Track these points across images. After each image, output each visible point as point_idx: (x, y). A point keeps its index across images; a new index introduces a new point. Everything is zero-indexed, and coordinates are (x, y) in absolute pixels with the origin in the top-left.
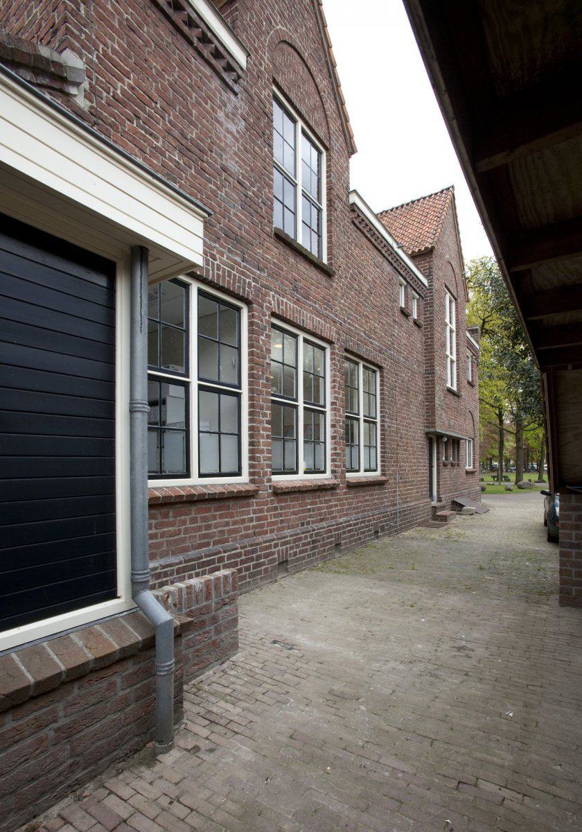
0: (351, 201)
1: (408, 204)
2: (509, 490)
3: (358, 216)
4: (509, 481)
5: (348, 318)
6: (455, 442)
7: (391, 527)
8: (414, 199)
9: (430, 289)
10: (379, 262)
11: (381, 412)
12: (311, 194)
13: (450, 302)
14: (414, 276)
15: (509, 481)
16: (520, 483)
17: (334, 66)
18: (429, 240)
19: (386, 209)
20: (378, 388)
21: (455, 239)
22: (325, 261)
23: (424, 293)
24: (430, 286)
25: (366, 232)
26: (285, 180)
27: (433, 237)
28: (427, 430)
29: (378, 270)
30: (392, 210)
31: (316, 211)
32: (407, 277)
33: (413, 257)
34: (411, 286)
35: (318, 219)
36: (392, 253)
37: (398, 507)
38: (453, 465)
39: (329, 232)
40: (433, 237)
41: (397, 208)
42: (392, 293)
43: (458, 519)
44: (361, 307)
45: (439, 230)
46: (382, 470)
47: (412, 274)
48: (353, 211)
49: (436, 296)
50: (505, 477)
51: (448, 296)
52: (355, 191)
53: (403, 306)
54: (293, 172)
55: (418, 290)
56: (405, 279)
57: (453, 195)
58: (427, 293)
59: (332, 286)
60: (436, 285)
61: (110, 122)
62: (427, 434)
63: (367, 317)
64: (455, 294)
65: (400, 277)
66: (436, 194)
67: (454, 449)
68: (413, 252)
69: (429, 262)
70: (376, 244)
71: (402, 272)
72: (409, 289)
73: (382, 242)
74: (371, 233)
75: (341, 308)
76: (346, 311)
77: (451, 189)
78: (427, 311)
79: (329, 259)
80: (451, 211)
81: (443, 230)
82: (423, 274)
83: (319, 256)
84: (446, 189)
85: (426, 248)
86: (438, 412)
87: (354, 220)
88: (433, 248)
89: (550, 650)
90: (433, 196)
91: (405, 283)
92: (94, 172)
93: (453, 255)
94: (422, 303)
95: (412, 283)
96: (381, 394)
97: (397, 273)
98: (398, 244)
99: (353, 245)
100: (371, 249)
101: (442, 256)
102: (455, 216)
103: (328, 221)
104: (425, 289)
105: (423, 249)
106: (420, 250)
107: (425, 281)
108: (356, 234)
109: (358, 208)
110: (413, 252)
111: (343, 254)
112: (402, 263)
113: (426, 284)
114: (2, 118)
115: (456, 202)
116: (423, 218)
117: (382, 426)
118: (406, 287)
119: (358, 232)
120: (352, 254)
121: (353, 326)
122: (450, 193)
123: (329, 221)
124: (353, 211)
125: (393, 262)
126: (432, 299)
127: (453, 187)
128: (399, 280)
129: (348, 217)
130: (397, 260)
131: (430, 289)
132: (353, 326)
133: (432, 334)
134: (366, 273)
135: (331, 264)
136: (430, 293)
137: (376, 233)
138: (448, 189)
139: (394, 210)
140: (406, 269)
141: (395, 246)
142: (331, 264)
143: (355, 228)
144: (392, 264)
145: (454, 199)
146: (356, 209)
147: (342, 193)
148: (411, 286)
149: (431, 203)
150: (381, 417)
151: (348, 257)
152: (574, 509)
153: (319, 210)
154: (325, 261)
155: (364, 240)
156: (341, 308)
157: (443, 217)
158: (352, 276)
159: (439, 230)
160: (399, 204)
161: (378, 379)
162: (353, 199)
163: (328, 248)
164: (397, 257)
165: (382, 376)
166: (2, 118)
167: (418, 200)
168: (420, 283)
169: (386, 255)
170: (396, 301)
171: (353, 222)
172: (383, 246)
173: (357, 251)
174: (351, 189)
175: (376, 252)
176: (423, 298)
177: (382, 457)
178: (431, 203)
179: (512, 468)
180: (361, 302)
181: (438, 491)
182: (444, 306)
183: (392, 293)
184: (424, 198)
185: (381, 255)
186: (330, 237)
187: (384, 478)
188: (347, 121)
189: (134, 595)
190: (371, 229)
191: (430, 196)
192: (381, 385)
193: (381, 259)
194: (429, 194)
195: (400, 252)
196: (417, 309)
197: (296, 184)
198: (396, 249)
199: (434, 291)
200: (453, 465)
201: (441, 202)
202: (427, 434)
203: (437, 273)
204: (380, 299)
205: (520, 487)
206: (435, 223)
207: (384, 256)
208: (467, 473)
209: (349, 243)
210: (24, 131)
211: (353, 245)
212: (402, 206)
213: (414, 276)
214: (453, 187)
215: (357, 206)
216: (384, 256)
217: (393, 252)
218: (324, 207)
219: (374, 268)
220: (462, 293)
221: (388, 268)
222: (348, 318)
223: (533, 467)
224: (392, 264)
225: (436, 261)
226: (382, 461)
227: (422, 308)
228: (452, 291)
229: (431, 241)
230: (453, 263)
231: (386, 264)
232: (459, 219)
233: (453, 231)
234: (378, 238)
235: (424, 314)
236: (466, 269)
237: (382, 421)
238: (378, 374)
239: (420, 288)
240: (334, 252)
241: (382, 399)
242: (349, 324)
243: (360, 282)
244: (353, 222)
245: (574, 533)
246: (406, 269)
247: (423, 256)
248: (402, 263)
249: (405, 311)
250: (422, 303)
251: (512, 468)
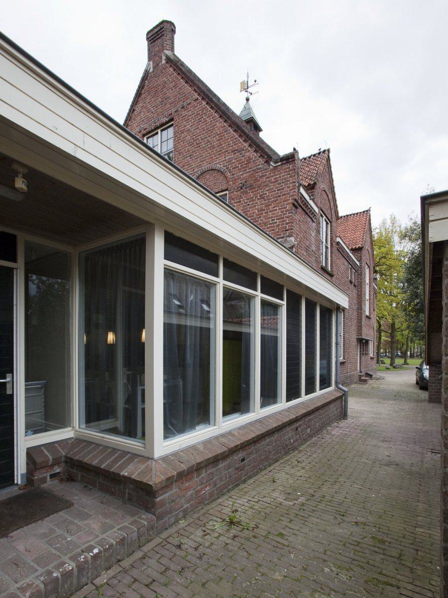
0: (337, 241)
2: (388, 369)
4: (384, 363)
6: (367, 341)
7: (347, 383)
9: (361, 267)
11: (343, 331)
14: (310, 208)
15: (384, 363)
16: (394, 365)
17: (334, 188)
20: (342, 320)
22: (329, 270)
28: (357, 337)
37: (348, 374)
38: (366, 354)
39: (331, 257)
43: (370, 382)
46: (343, 357)
48: (338, 244)
50: (381, 361)
57: (329, 156)
62: (357, 339)
64: (329, 217)
66: (361, 213)
67: (366, 346)
86: (364, 328)
88: (363, 247)
89: (400, 507)
92: (99, 141)
94: (356, 274)
96: (344, 322)
105: (357, 247)
106: (355, 248)
107: (358, 263)
113: (359, 265)
114: (1, 78)
117: (344, 337)
118: (351, 269)
124: (338, 244)
127: (328, 150)
133: (361, 290)
150: (343, 333)
152: (434, 371)
154: (329, 270)
159: (365, 237)
161: (342, 315)
165: (344, 314)
166: (1, 78)
167: (351, 215)
177: (343, 351)
179: (382, 355)
181: (360, 368)
184: (354, 214)
186: (331, 259)
187: (345, 361)
188: (337, 207)
189: (336, 386)
192: (344, 318)
194: (356, 212)
200: (366, 354)
202: (357, 339)
205: (394, 367)
208: (371, 358)
210: (58, 115)
223: (398, 355)
226: (343, 353)
237: (344, 335)
238: (342, 313)
241: (344, 325)
245: (434, 379)
246: (307, 206)
247: (357, 250)
250: (356, 274)
251: (382, 355)
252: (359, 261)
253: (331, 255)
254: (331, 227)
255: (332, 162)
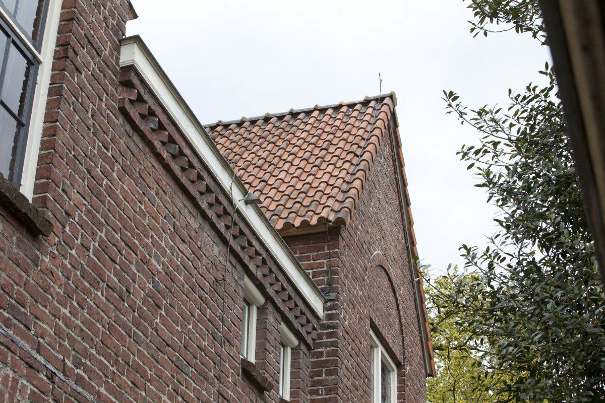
1: (281, 118)
3: (140, 99)
5: (78, 364)
8: (297, 108)
9: (330, 326)
10: (188, 226)
12: (14, 17)
13: (385, 370)
14: (286, 284)
18: (330, 202)
19: (225, 120)
21: (397, 215)
22: (27, 189)
23: (314, 334)
24: (329, 317)
25: (157, 145)
26: (12, 47)
27: (340, 197)
29: (183, 247)
30: (240, 124)
31: (23, 63)
32: (266, 282)
33: (290, 237)
34: (277, 309)
35: (25, 83)
36: (226, 213)
39: (50, 118)
40: (340, 197)
41: (253, 122)
42: (222, 319)
44: (121, 338)
45: (357, 183)
47: (281, 277)
48: (127, 84)
49: (345, 349)
51: (379, 353)
52: (137, 39)
53: (252, 359)
54: (30, 29)
55: (296, 324)
56: (261, 287)
57: (393, 115)
58: (320, 336)
59: (36, 262)
60: (347, 319)
61: (193, 297)
63: (137, 369)
64: (397, 351)
65: (247, 281)
68: (288, 226)
69: (329, 256)
70: (184, 180)
71: (252, 267)
72: (271, 317)
73: (200, 178)
74: (174, 149)
75: (57, 328)
76: (72, 341)
77: (387, 101)
78: (320, 383)
79: (37, 188)
80: (387, 150)
81: (366, 186)
82: (313, 285)
83: (11, 176)
84: (376, 100)
85: (322, 221)
87: (128, 106)
88: (340, 222)
90: (344, 109)
91: (261, 300)
93: (392, 252)
94: (306, 360)
95: (279, 301)
97: (239, 268)
98: (245, 192)
99: (117, 167)
100: (168, 189)
101: (363, 249)
102: (398, 163)
103: (51, 92)
104: (314, 321)
105: (314, 222)
106: (305, 224)
107: (317, 304)
108: (126, 141)
109: (142, 81)
110: (288, 226)
111: (83, 184)
112: (255, 243)
115: (401, 130)
116: (316, 151)
118: (261, 310)
119: (136, 138)
120: (111, 193)
121: (91, 390)
122: (385, 108)
123: (55, 91)
125: (228, 236)
126: (334, 353)
127: (392, 97)
128: (245, 289)
129: (112, 96)
130: (242, 233)
131: (329, 327)
132: (91, 390)
134: (146, 246)
135: (44, 201)
136: (330, 335)
137: (187, 151)
138: (380, 100)
139: (246, 124)
140: (264, 262)
141: (237, 195)
142: (44, 201)
143: (128, 128)
144: (225, 241)
145: (396, 125)
146: (136, 81)
147: (101, 35)
148: (277, 309)
149: (337, 123)
151: (98, 196)
153: (33, 63)
154: (27, 189)
155: (150, 161)
156: (57, 328)
157: (367, 156)
158: (105, 249)
160: (260, 113)
162: (130, 55)
163: (41, 158)
164: (171, 129)
167: (308, 113)
168: (301, 305)
169: (210, 213)
170: (232, 340)
171: (123, 112)
172: (203, 188)
173: (127, 184)
174: (128, 34)
175: (180, 201)
176: (309, 348)
178: (337, 123)
180: (124, 326)
182: (369, 378)
183: (222, 319)
184: (323, 111)
185: (195, 212)
186: (50, 133)
190: (171, 140)
191: (337, 108)
193: (195, 223)
194: (336, 103)
195: (250, 214)
196: (292, 374)
197: (39, 62)
198: (241, 206)
199: (340, 332)
201: (364, 125)
203: (349, 289)
204: (184, 327)
206: (346, 166)
207: (204, 216)
209: (105, 158)
211: (117, 167)
212: (267, 119)
213: (286, 284)
214: (392, 97)
215: (138, 74)
216: (204, 216)
217: (229, 209)
218: (47, 55)
219: (171, 240)
220: (415, 352)
221: (216, 250)
222: (78, 364)
224: (225, 241)
225: (347, 257)
227: (305, 373)
228: (390, 340)
229: (337, 206)
230: (391, 271)
231: (207, 237)
232: (408, 170)
233: (392, 195)
234: (191, 166)
235: (313, 392)
236: (428, 304)
239: (304, 321)
240: (57, 172)
242: (79, 380)
243: (125, 268)
244: (123, 112)
246: (264, 262)
247: (314, 238)
248: (255, 243)
249: (259, 374)
250: (306, 360)
252: (320, 293)
253: (50, 105)
254: (399, 382)
255: (402, 130)
